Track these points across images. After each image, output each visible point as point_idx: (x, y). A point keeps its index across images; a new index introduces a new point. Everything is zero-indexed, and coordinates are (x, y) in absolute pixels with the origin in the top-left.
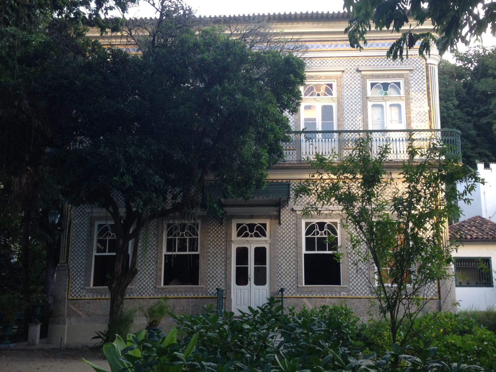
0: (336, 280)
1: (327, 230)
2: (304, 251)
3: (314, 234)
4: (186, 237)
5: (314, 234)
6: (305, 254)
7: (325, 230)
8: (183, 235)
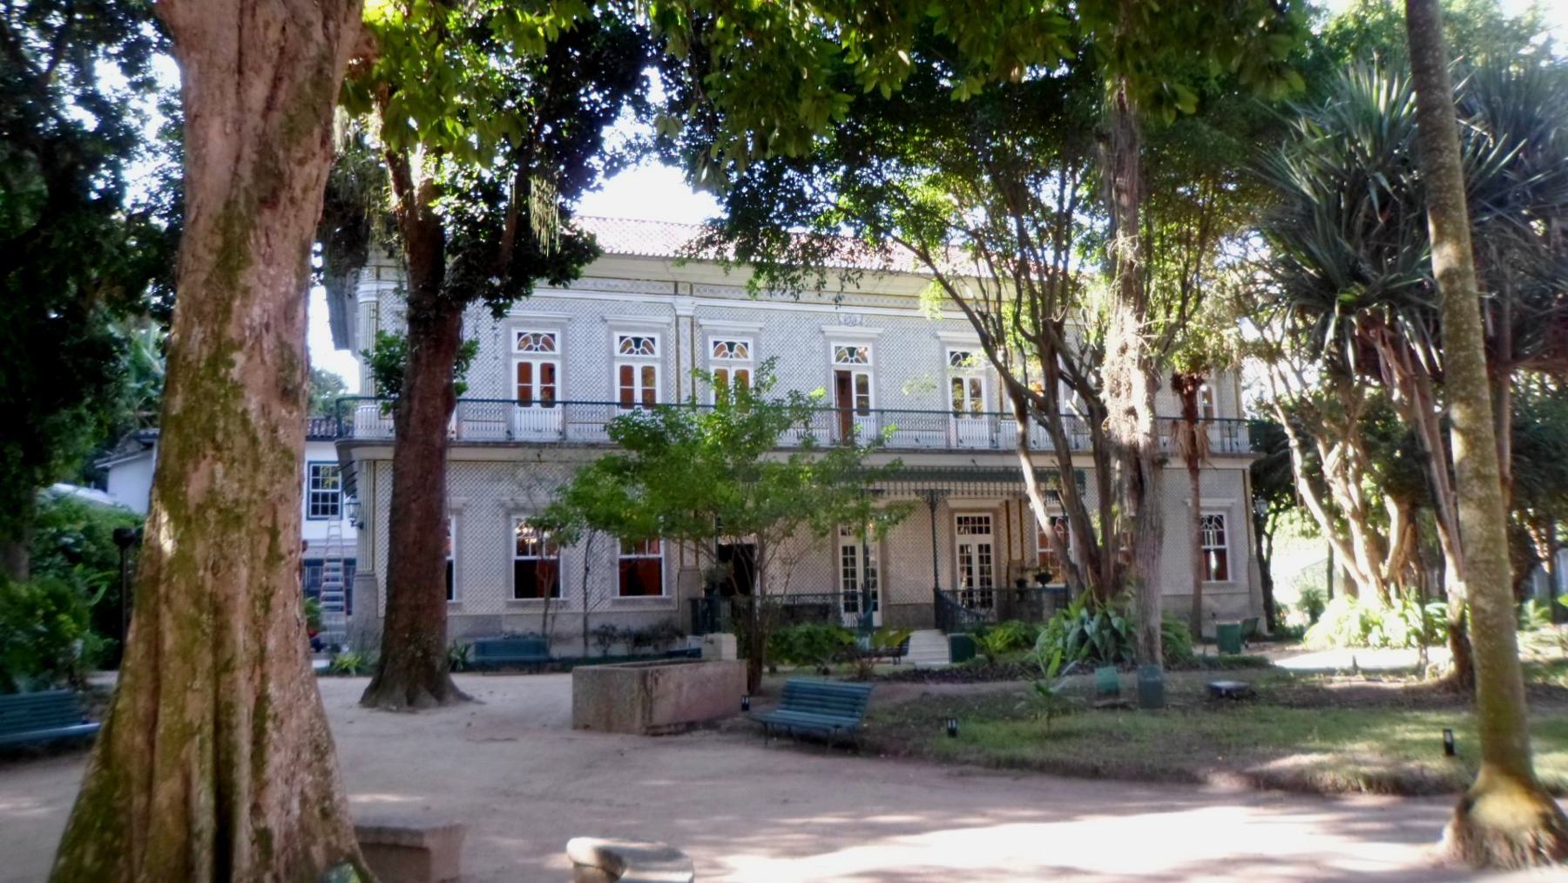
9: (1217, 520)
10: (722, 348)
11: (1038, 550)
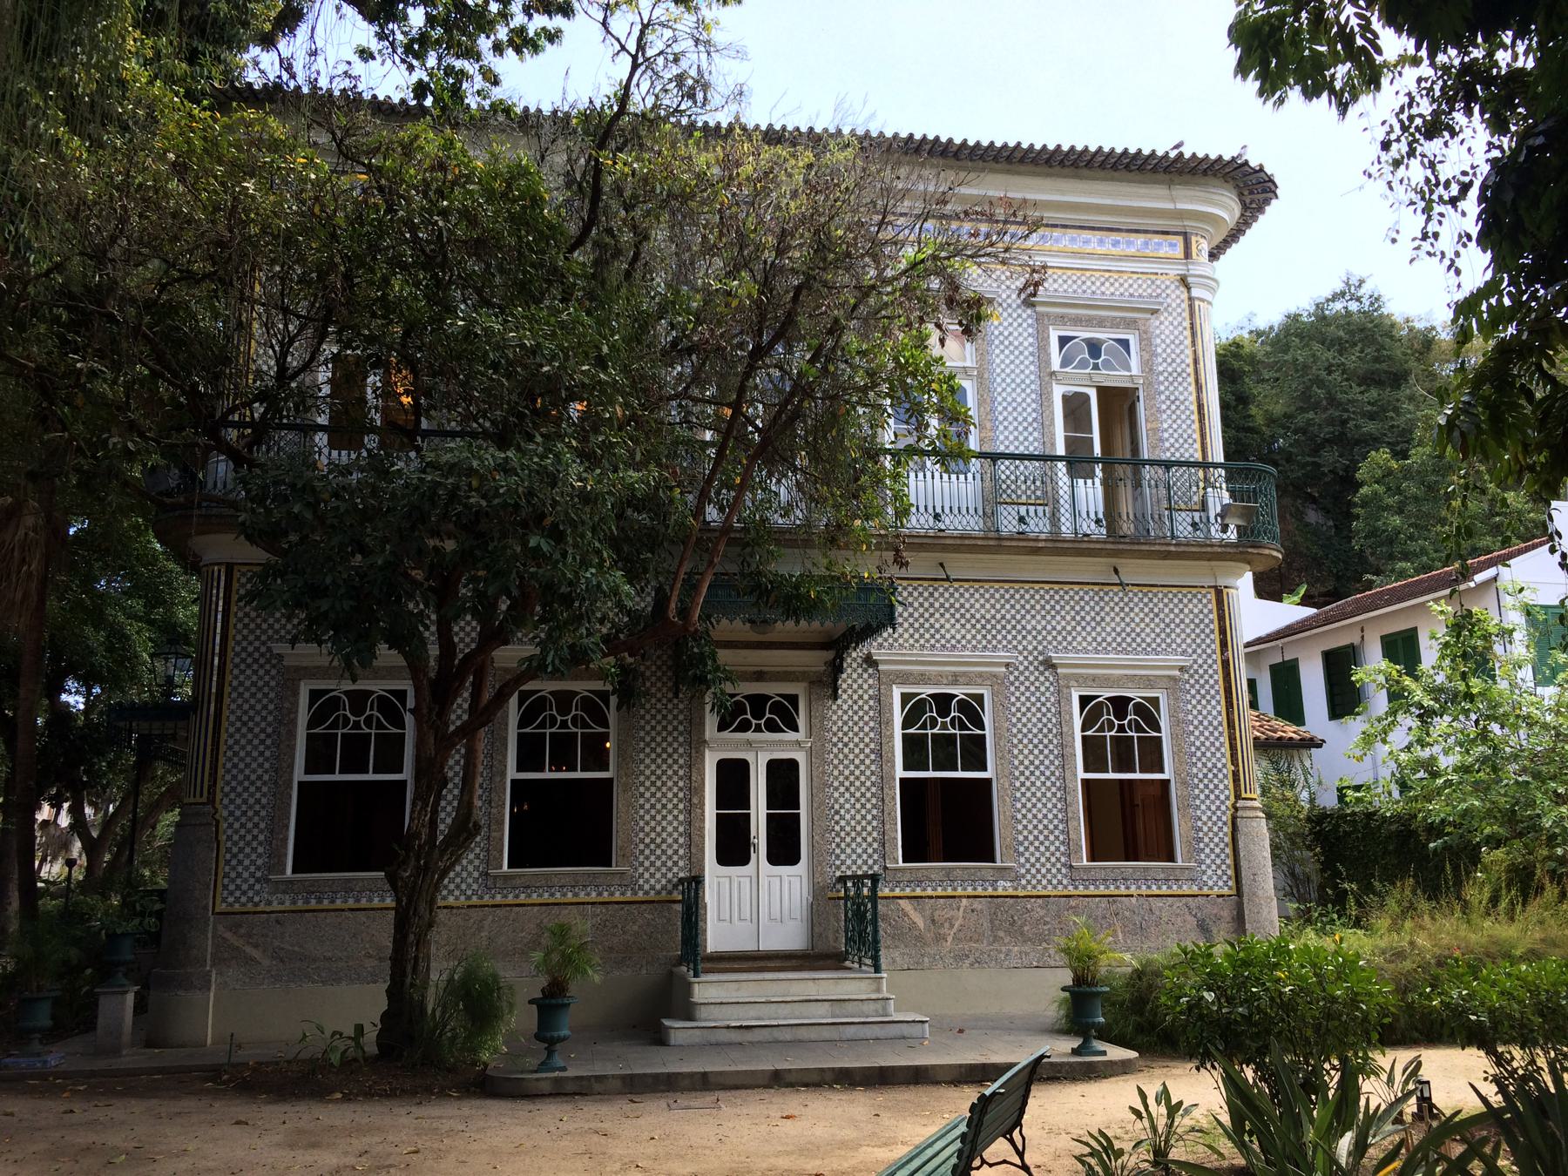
0: (603, 857)
1: (375, 713)
2: (299, 775)
3: (924, 727)
4: (575, 730)
5: (1101, 729)
7: (573, 713)
8: (564, 724)
9: (964, 706)
11: (1081, 774)
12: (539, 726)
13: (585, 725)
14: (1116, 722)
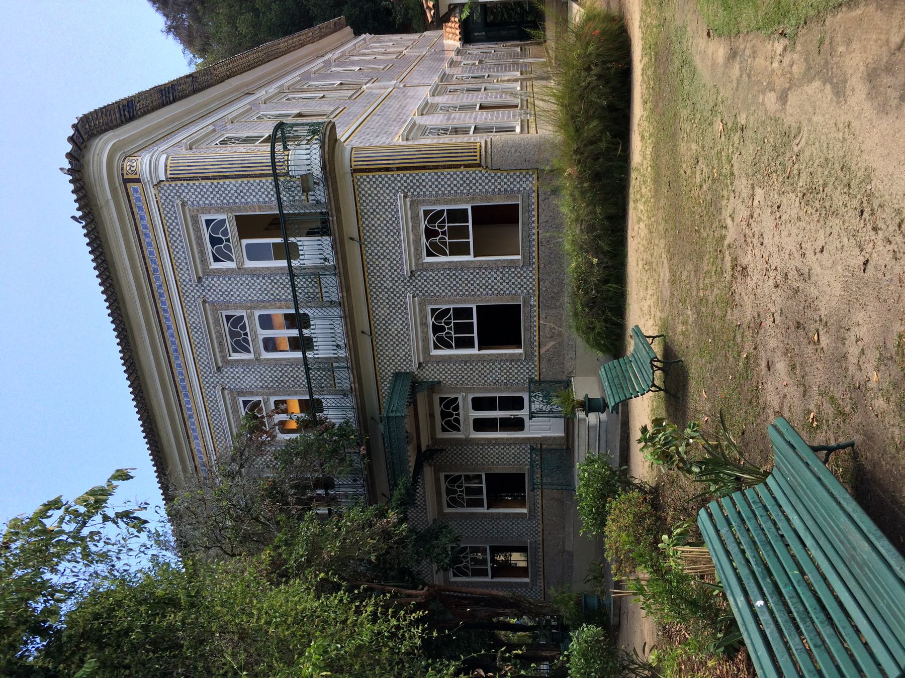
0: (514, 310)
6: (475, 256)
10: (219, 250)
12: (468, 569)
13: (450, 318)
14: (440, 236)
